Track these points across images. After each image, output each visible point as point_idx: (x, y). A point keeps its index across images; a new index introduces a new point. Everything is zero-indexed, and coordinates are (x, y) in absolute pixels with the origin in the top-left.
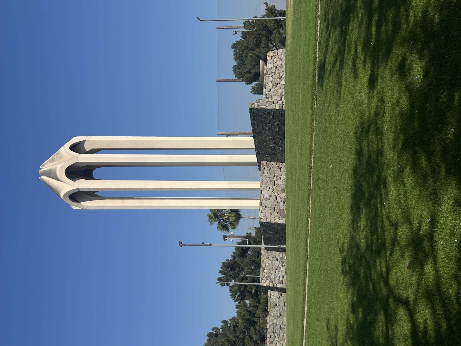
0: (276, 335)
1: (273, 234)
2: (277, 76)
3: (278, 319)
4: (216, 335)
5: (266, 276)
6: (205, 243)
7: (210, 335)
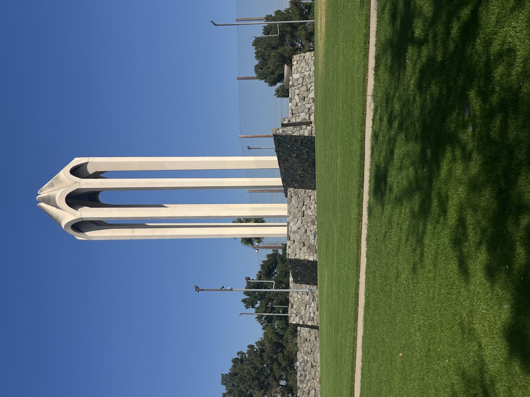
0: (307, 373)
2: (304, 88)
3: (310, 355)
4: (242, 361)
5: (295, 312)
6: (225, 288)
7: (235, 361)
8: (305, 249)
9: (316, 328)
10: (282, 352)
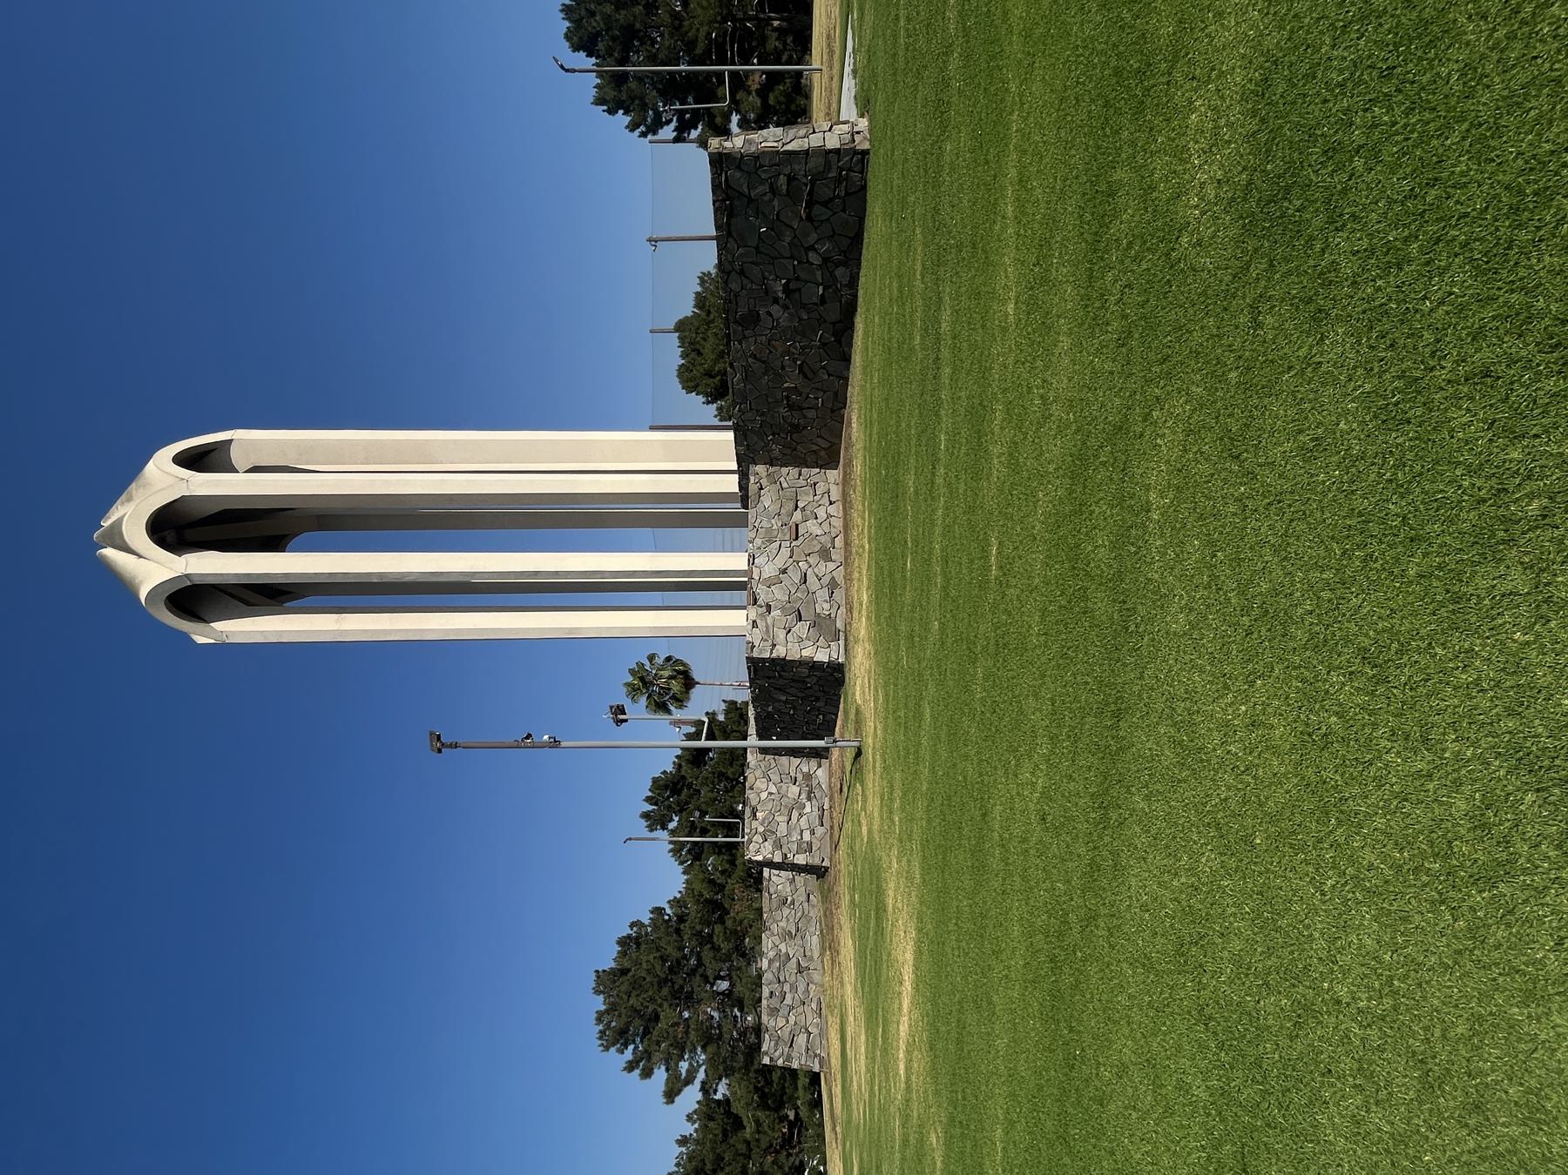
0: (787, 988)
1: (797, 699)
5: (761, 829)
7: (623, 942)
8: (802, 629)
9: (819, 872)
10: (721, 920)
